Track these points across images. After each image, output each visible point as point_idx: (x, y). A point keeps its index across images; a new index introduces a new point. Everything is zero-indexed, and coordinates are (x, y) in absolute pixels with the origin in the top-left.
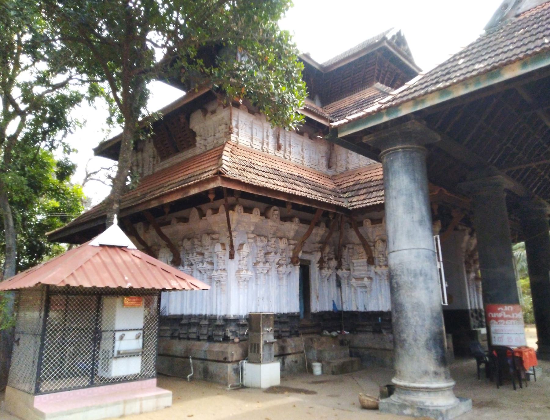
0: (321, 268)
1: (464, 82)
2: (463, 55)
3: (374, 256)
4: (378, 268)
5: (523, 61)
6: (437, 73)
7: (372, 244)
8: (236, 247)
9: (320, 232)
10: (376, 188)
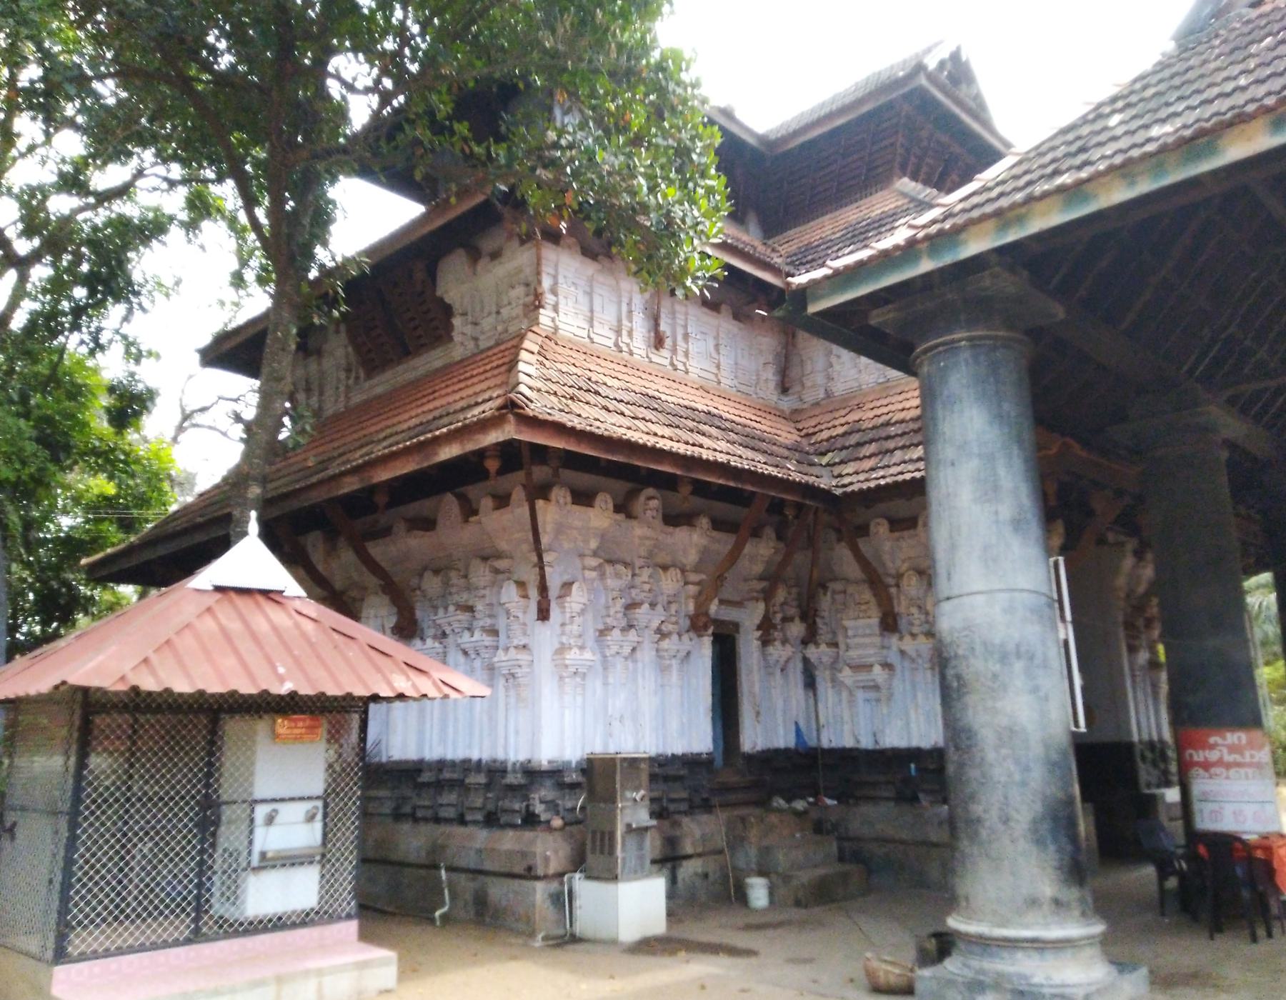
0: (765, 642)
1: (1125, 170)
2: (1120, 104)
3: (896, 610)
4: (907, 638)
6: (1053, 149)
7: (891, 581)
8: (553, 591)
9: (761, 552)
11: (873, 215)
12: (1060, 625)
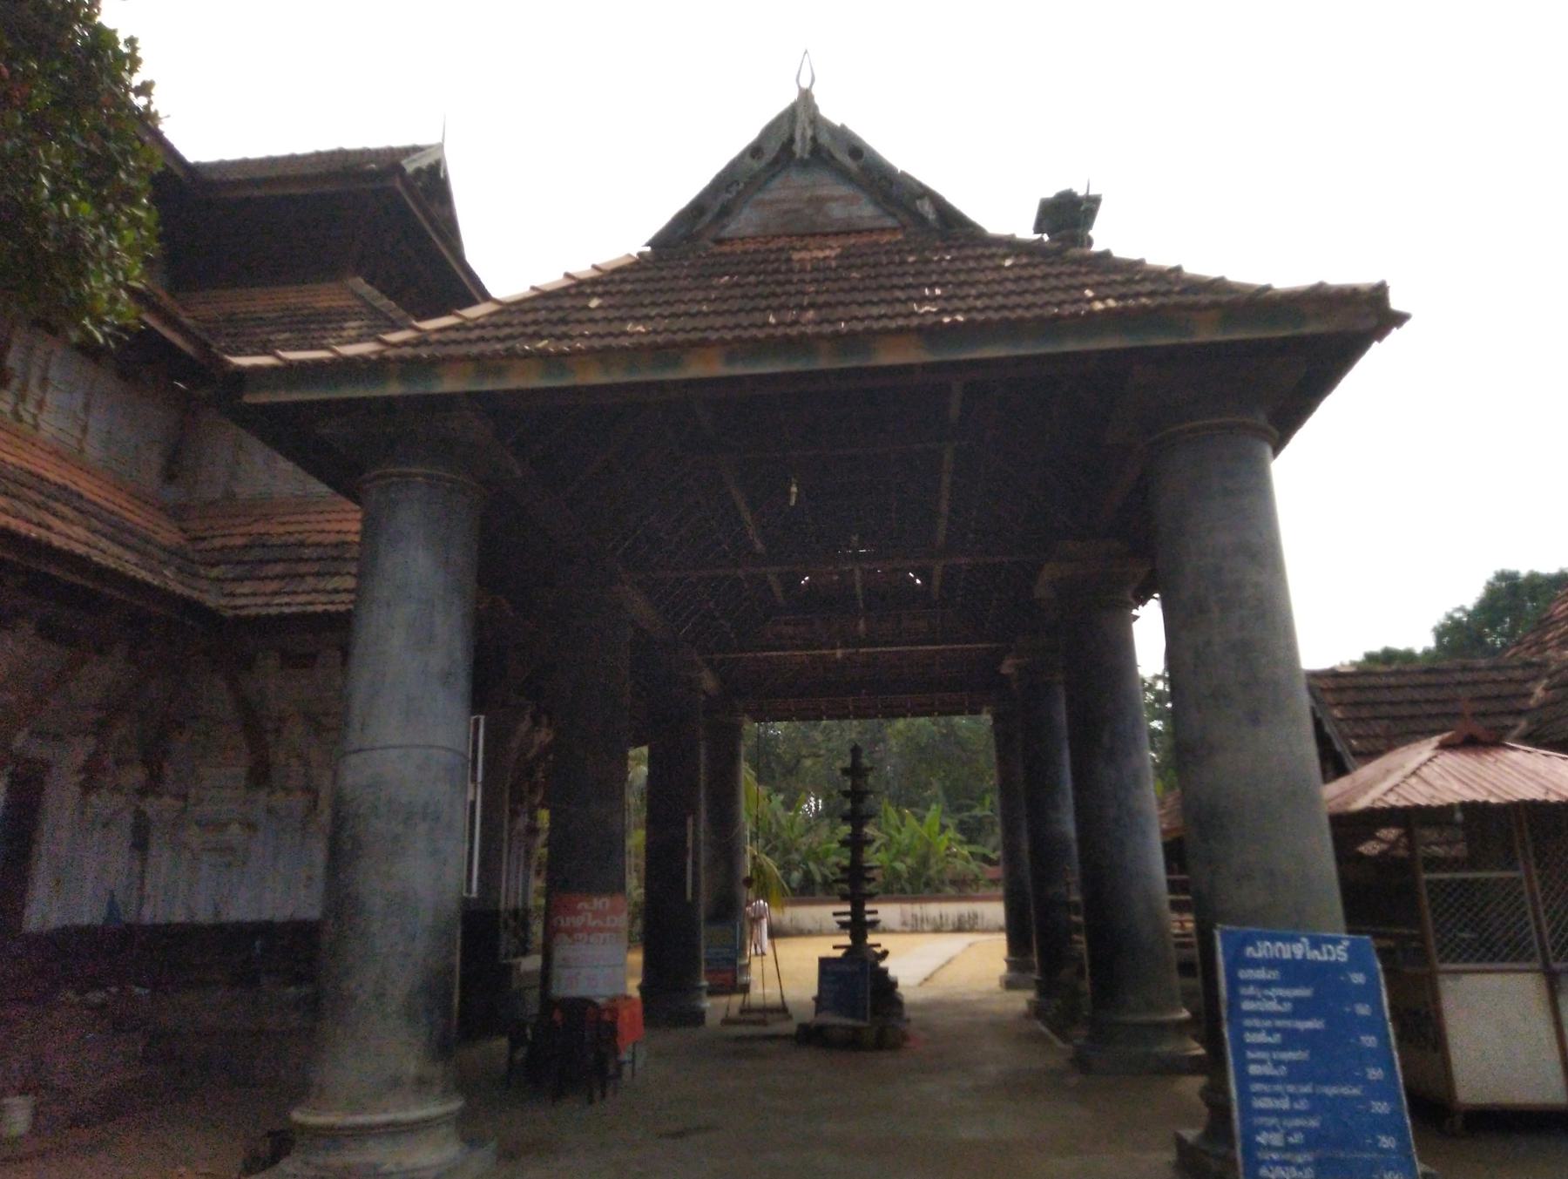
0: (88, 787)
1: (603, 356)
2: (600, 289)
4: (280, 794)
5: (735, 349)
6: (536, 310)
7: (270, 726)
9: (102, 675)
10: (316, 568)
11: (318, 305)
12: (470, 786)
